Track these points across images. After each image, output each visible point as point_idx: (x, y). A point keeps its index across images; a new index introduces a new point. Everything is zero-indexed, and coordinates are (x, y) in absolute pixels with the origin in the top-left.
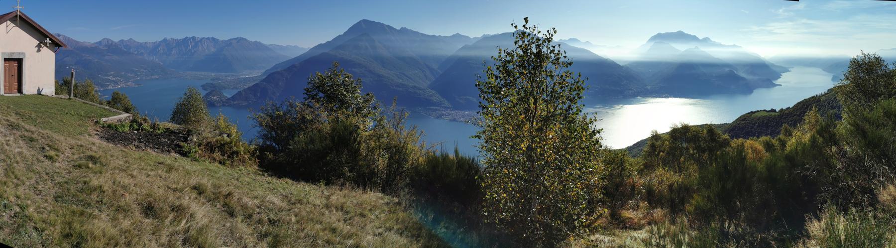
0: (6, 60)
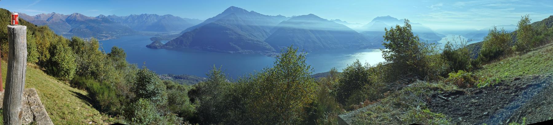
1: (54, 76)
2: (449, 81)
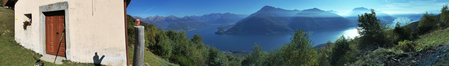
0: (47, 14)
1: (159, 55)
2: (399, 47)
